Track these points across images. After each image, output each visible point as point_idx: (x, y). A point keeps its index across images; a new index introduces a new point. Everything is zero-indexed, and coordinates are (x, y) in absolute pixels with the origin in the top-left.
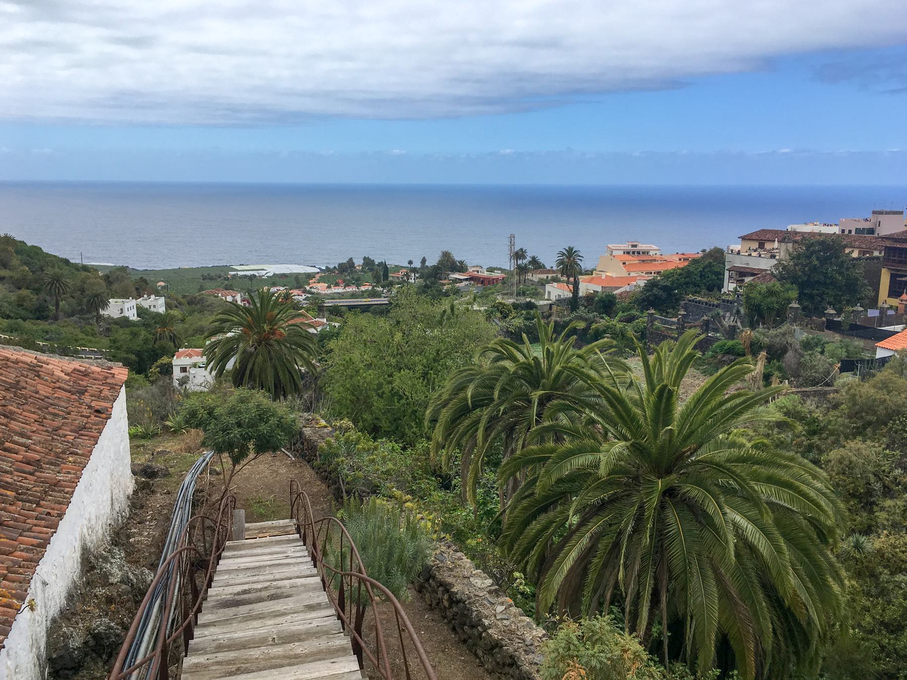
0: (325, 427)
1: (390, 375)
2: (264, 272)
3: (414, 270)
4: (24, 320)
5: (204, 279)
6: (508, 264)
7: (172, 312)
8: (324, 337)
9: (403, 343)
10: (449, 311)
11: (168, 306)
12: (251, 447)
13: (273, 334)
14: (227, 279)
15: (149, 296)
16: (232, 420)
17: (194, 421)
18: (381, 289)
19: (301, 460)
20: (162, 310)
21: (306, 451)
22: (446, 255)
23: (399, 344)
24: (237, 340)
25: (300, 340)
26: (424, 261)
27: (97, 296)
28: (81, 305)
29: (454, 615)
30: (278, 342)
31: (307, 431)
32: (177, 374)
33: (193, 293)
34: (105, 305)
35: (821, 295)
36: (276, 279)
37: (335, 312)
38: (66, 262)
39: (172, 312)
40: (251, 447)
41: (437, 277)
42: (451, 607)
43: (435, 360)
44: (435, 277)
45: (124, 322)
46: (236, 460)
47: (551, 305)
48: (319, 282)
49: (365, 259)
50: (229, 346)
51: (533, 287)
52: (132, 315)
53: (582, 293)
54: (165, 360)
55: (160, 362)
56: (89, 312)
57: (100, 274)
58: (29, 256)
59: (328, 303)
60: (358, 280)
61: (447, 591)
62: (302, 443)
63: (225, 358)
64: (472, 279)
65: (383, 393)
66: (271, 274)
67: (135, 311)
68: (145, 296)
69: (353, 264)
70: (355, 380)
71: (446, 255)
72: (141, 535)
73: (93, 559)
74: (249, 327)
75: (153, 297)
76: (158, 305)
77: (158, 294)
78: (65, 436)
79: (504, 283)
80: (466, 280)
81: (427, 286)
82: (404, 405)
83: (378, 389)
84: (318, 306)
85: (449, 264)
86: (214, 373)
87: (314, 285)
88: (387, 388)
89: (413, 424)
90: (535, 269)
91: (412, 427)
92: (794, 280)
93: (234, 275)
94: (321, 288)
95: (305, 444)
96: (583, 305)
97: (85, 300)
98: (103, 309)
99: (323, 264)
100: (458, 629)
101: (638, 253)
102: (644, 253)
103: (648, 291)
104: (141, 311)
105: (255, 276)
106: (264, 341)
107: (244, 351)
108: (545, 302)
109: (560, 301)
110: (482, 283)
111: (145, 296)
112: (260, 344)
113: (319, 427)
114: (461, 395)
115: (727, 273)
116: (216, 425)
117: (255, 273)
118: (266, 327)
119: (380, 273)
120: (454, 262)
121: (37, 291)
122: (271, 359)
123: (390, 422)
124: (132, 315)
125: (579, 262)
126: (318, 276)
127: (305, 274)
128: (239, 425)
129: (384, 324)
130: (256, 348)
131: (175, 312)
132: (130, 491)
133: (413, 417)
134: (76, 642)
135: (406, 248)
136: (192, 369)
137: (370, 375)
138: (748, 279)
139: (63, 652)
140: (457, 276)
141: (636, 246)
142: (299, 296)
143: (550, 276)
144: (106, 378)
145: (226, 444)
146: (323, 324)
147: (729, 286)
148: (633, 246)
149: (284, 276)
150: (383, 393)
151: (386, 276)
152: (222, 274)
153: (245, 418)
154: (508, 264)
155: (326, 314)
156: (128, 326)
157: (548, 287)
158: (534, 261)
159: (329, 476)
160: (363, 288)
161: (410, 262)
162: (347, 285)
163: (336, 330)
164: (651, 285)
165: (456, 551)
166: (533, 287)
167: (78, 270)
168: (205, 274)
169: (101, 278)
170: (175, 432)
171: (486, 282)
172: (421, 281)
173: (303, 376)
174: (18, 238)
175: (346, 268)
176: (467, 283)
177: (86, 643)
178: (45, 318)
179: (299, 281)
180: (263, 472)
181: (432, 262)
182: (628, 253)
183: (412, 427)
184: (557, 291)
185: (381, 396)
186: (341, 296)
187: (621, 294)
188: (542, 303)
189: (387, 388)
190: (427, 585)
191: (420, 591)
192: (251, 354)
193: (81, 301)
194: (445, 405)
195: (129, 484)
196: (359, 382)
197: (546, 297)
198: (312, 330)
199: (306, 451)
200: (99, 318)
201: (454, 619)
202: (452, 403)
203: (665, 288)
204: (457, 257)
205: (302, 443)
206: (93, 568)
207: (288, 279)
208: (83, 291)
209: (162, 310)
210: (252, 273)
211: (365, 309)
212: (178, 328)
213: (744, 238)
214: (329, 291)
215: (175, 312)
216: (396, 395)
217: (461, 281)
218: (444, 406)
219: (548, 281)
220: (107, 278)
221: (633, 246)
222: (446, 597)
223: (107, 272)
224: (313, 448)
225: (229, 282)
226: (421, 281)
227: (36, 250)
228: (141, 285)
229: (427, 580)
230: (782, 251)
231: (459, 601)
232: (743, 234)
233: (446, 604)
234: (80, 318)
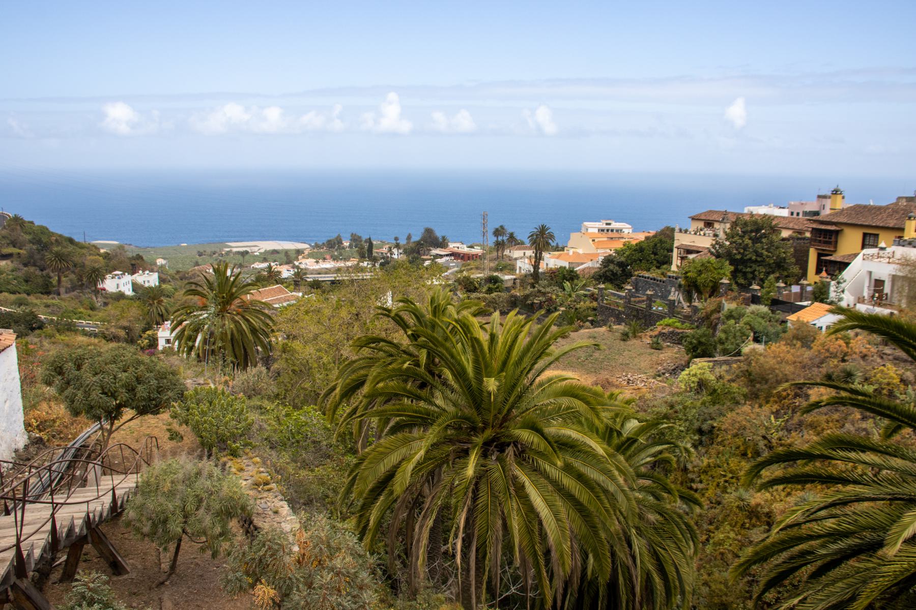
2: (256, 249)
4: (28, 294)
7: (164, 286)
11: (162, 280)
22: (429, 231)
26: (409, 237)
35: (753, 273)
38: (71, 241)
39: (164, 286)
45: (120, 296)
52: (128, 291)
53: (542, 268)
57: (102, 251)
66: (262, 251)
67: (130, 286)
68: (141, 272)
71: (429, 231)
75: (147, 272)
76: (150, 279)
80: (447, 255)
87: (304, 261)
92: (729, 256)
94: (308, 264)
99: (312, 241)
101: (612, 231)
102: (617, 231)
103: (605, 267)
111: (141, 272)
115: (675, 250)
117: (248, 249)
120: (436, 238)
124: (128, 291)
126: (306, 252)
132: (21, 445)
138: (691, 257)
141: (609, 224)
147: (676, 262)
148: (607, 224)
149: (275, 252)
152: (218, 250)
158: (512, 236)
161: (396, 239)
164: (608, 261)
165: (281, 500)
171: (466, 258)
174: (27, 219)
176: (447, 258)
178: (48, 293)
181: (416, 238)
182: (603, 230)
186: (327, 271)
187: (583, 270)
195: (22, 440)
200: (97, 292)
203: (621, 265)
204: (439, 234)
207: (278, 255)
210: (245, 249)
213: (693, 219)
214: (317, 267)
217: (441, 256)
221: (607, 224)
227: (44, 230)
230: (722, 229)
232: (692, 215)
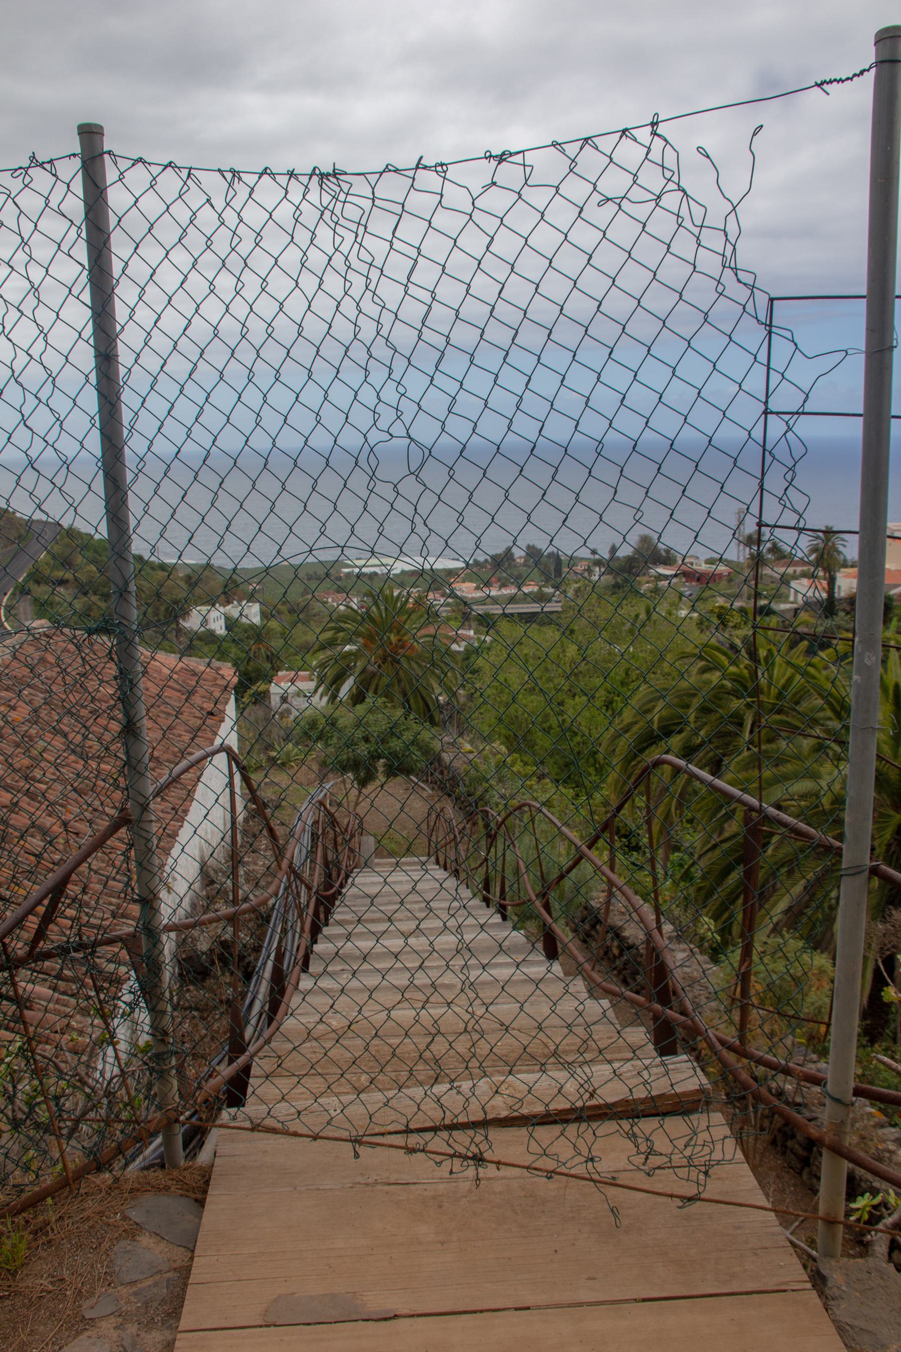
0: (471, 752)
1: (561, 704)
3: (598, 563)
5: (309, 579)
6: (738, 554)
8: (472, 652)
9: (579, 659)
10: (643, 616)
11: (264, 615)
12: (381, 769)
13: (402, 647)
14: (340, 579)
15: (240, 601)
16: (359, 734)
17: (314, 734)
18: (551, 590)
19: (440, 793)
20: (257, 620)
21: (446, 782)
23: (573, 661)
24: (355, 655)
25: (438, 658)
26: (613, 550)
27: (176, 602)
28: (157, 615)
29: (625, 964)
30: (409, 659)
31: (446, 757)
32: (275, 701)
33: (294, 594)
34: (186, 614)
36: (403, 579)
37: (486, 622)
40: (381, 769)
41: (627, 572)
42: (621, 954)
43: (623, 683)
44: (630, 572)
46: (363, 783)
47: (796, 610)
48: (464, 582)
49: (529, 547)
50: (343, 663)
51: (773, 586)
52: (218, 627)
54: (261, 686)
55: (254, 688)
56: (167, 624)
58: (96, 551)
59: (479, 609)
60: (518, 577)
61: (617, 935)
62: (442, 773)
63: (339, 679)
64: (685, 574)
65: (550, 727)
67: (222, 622)
69: (512, 555)
70: (512, 710)
72: (256, 864)
73: (212, 873)
74: (370, 637)
76: (253, 613)
77: (251, 597)
78: (180, 736)
79: (730, 580)
81: (617, 586)
82: (578, 743)
83: (544, 722)
84: (464, 612)
85: (650, 554)
86: (325, 699)
88: (554, 721)
89: (591, 770)
90: (778, 559)
91: (590, 775)
93: (349, 573)
94: (467, 589)
95: (446, 772)
96: (844, 610)
97: (163, 608)
98: (184, 620)
100: (629, 980)
104: (231, 624)
105: (376, 574)
106: (390, 658)
107: (363, 671)
108: (788, 606)
109: (807, 605)
110: (698, 580)
112: (384, 660)
113: (462, 751)
114: (649, 717)
116: (339, 739)
118: (393, 638)
119: (551, 567)
121: (106, 597)
122: (399, 681)
123: (559, 767)
124: (218, 627)
125: (841, 548)
127: (444, 570)
128: (366, 740)
129: (551, 634)
130: (379, 667)
131: (273, 624)
133: (591, 760)
134: (203, 946)
135: (593, 534)
136: (296, 692)
137: (534, 702)
139: (191, 953)
140: (662, 570)
142: (436, 599)
143: (799, 569)
144: (216, 679)
145: (351, 763)
146: (470, 638)
150: (550, 727)
151: (558, 571)
153: (374, 730)
154: (738, 554)
155: (474, 624)
156: (213, 642)
157: (794, 584)
159: (472, 807)
160: (526, 590)
162: (503, 586)
163: (487, 645)
166: (773, 586)
167: (153, 569)
168: (311, 573)
169: (181, 579)
170: (283, 764)
172: (608, 579)
173: (440, 707)
175: (502, 561)
177: (211, 950)
179: (436, 580)
180: (393, 802)
183: (590, 775)
184: (803, 589)
185: (547, 731)
188: (783, 607)
189: (554, 721)
190: (593, 933)
191: (584, 941)
192: (374, 675)
193: (158, 609)
194: (627, 729)
196: (516, 711)
197: (792, 599)
198: (455, 647)
199: (446, 782)
200: (179, 631)
201: (625, 969)
202: (638, 726)
205: (442, 773)
206: (212, 882)
208: (158, 595)
209: (257, 620)
211: (529, 618)
212: (277, 644)
215: (273, 624)
216: (568, 731)
217: (666, 577)
218: (626, 731)
219: (795, 577)
220: (188, 578)
222: (616, 943)
223: (188, 571)
224: (455, 781)
225: (344, 586)
226: (608, 579)
228: (230, 588)
229: (593, 927)
231: (630, 947)
233: (616, 952)
234: (156, 632)
